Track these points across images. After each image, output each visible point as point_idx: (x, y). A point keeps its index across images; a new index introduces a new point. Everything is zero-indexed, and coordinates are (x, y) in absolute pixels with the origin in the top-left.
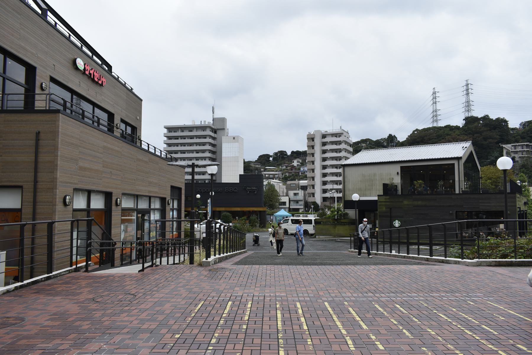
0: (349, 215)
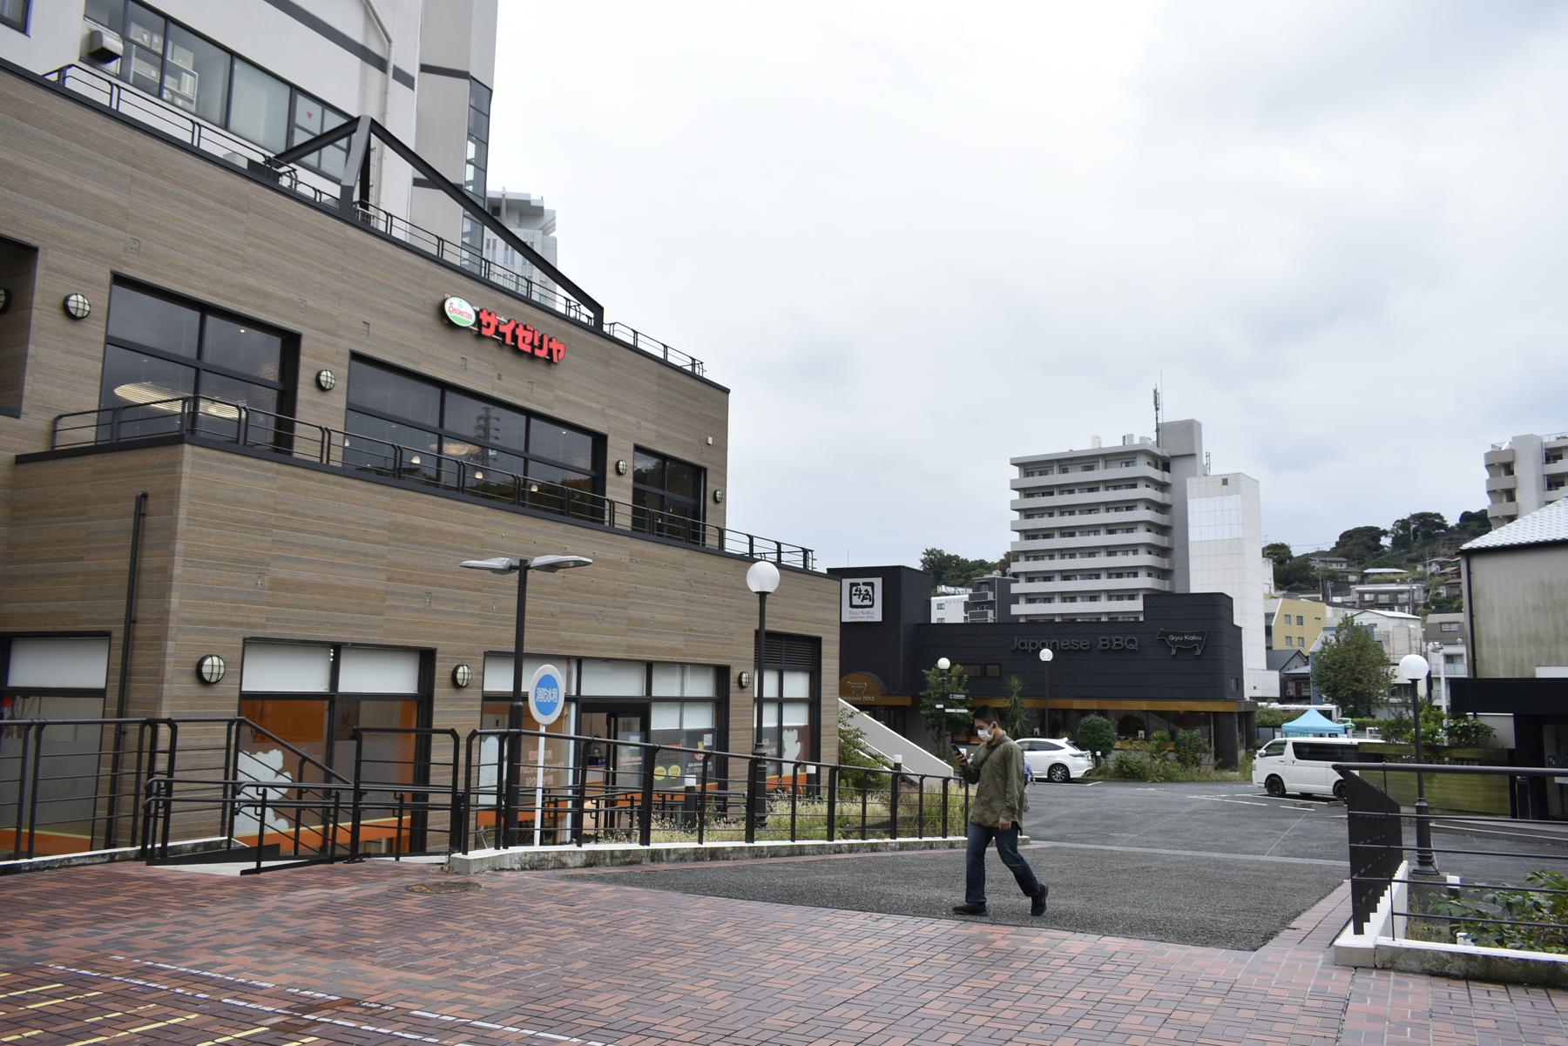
0: (1495, 732)
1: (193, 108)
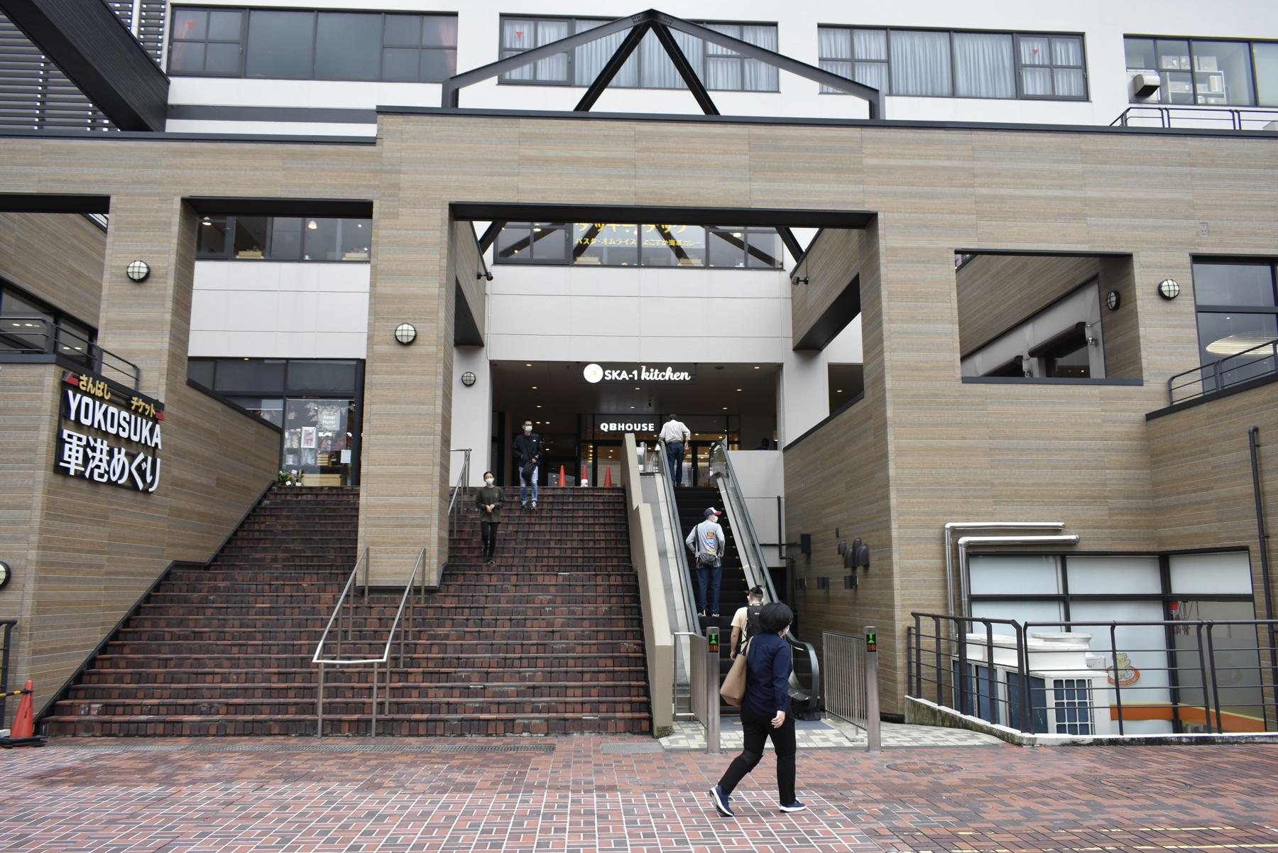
1: (1224, 101)
